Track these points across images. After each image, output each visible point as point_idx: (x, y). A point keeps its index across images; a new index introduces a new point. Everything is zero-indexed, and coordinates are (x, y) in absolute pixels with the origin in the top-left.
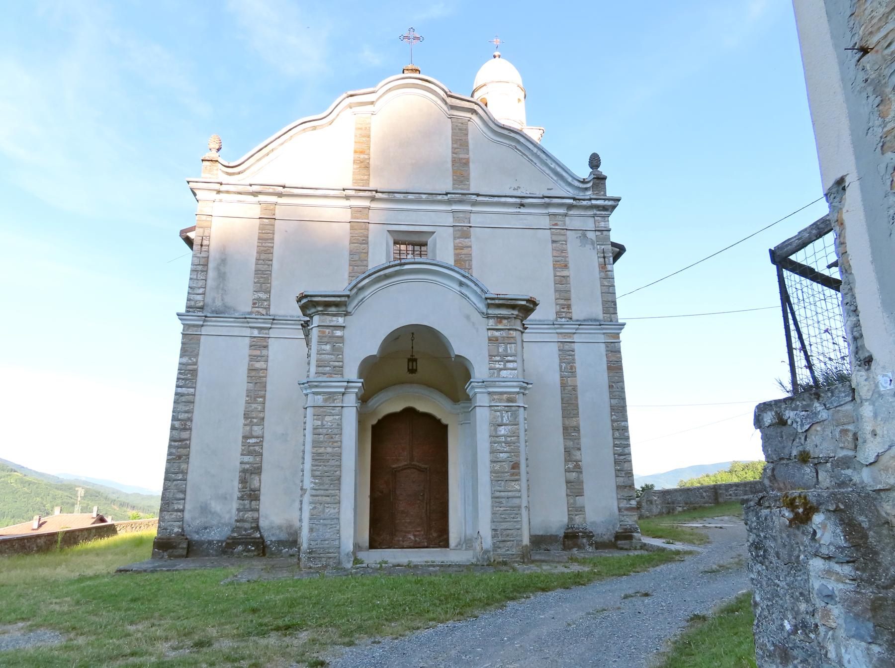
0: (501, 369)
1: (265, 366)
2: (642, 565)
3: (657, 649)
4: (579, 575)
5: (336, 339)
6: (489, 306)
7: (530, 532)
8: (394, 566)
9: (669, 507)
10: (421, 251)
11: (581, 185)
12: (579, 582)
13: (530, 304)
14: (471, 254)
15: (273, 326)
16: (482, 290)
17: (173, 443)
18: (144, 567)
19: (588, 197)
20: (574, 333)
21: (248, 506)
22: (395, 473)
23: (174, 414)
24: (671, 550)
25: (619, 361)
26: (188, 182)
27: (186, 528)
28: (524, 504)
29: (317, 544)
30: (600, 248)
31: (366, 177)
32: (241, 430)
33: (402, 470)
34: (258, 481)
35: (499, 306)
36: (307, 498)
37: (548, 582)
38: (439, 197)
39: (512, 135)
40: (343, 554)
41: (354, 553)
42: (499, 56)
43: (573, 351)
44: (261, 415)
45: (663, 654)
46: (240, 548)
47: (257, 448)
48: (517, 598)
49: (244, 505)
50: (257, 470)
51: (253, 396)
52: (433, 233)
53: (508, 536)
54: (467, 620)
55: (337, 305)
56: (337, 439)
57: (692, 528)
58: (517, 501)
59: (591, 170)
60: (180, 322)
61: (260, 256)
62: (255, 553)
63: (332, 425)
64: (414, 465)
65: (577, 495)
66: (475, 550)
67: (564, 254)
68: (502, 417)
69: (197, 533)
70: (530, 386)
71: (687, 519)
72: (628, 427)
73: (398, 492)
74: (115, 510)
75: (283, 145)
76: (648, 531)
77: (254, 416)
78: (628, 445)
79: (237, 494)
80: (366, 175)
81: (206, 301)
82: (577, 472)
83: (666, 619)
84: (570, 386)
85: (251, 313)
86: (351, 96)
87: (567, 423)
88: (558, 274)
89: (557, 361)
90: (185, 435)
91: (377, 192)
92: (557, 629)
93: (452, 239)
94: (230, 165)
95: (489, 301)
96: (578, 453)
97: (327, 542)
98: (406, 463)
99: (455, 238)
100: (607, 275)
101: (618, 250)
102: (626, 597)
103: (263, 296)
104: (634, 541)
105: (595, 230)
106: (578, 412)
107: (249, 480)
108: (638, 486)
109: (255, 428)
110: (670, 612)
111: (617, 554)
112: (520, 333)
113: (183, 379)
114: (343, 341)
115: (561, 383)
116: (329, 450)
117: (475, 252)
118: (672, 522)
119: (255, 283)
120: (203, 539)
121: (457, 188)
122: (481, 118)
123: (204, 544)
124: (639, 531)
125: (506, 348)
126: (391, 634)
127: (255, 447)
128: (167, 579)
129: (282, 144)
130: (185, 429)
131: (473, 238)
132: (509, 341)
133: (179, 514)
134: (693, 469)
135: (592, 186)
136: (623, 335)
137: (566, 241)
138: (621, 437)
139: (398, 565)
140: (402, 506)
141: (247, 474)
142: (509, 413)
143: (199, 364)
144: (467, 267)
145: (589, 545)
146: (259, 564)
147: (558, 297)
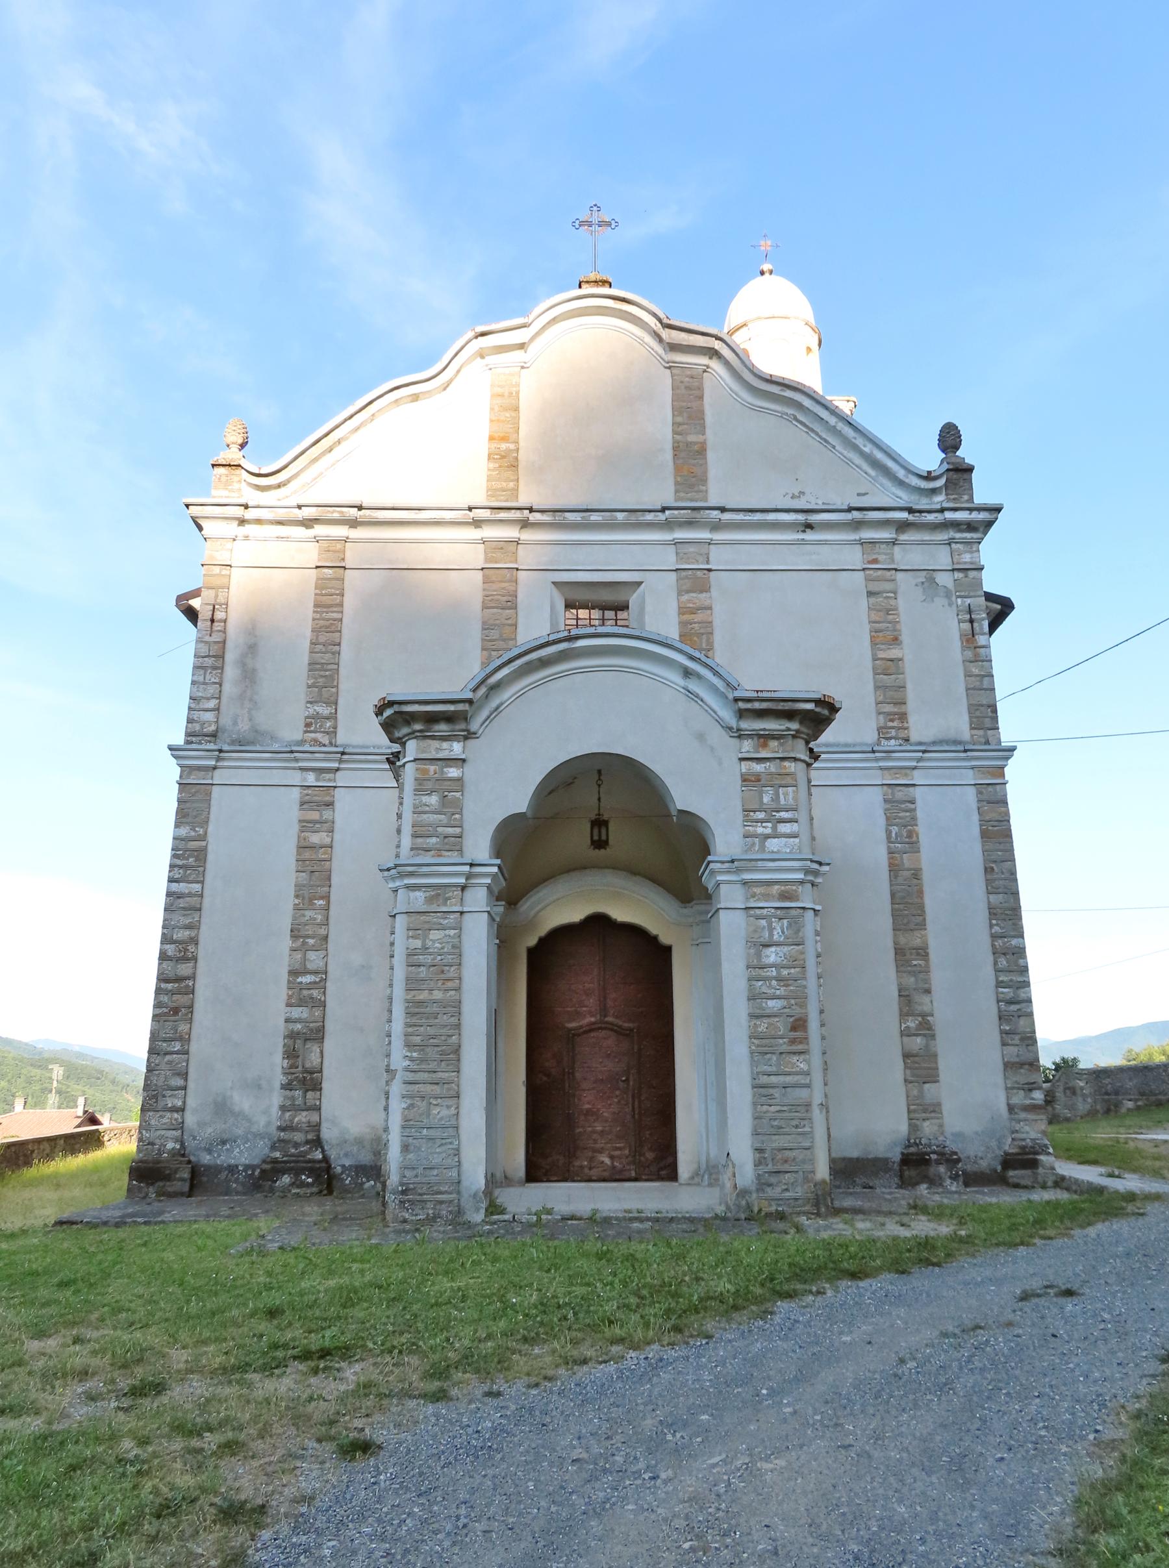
0: (767, 837)
1: (327, 840)
2: (1057, 1224)
3: (1097, 1431)
4: (926, 1243)
5: (449, 783)
6: (741, 714)
7: (830, 1155)
8: (564, 1219)
9: (1109, 1100)
10: (616, 620)
11: (924, 484)
12: (927, 1259)
13: (823, 708)
14: (711, 622)
15: (342, 766)
16: (728, 684)
17: (163, 985)
18: (105, 1215)
19: (938, 507)
20: (915, 768)
21: (299, 1101)
22: (572, 1037)
23: (165, 931)
24: (1117, 1192)
25: (1005, 819)
26: (187, 506)
27: (190, 1144)
28: (818, 1098)
29: (416, 1176)
30: (963, 602)
31: (511, 485)
32: (287, 959)
33: (586, 1032)
34: (318, 1054)
35: (761, 714)
36: (396, 1088)
37: (863, 1258)
38: (650, 517)
39: (788, 394)
40: (465, 1195)
41: (488, 1192)
42: (771, 272)
43: (913, 802)
44: (323, 932)
45: (1112, 1445)
46: (286, 1179)
47: (315, 993)
48: (796, 1295)
49: (293, 1098)
50: (317, 1035)
51: (307, 896)
52: (639, 584)
53: (786, 1161)
54: (687, 1343)
55: (449, 718)
56: (451, 975)
57: (1156, 1144)
58: (803, 1094)
59: (944, 456)
60: (174, 761)
61: (317, 637)
62: (315, 1190)
63: (443, 948)
64: (607, 1023)
65: (925, 1080)
66: (722, 1187)
67: (891, 617)
68: (771, 930)
69: (209, 1151)
70: (825, 868)
71: (1144, 1123)
72: (1024, 948)
73: (578, 1075)
74: (128, 1101)
75: (359, 432)
76: (1068, 1150)
77: (310, 933)
78: (1026, 984)
79: (279, 1078)
80: (512, 481)
81: (222, 721)
82: (924, 1035)
83: (1112, 1352)
84: (908, 870)
85: (302, 742)
86: (483, 334)
87: (902, 940)
88: (881, 655)
89: (882, 821)
90: (184, 969)
91: (531, 510)
92: (874, 1372)
93: (674, 595)
94: (262, 472)
95: (741, 705)
96: (926, 999)
97: (435, 1172)
98: (593, 1019)
99: (680, 593)
100: (976, 655)
101: (999, 607)
102: (1025, 1297)
103: (324, 710)
104: (1040, 1170)
105: (953, 570)
106: (925, 919)
107: (301, 1053)
108: (1047, 1060)
109: (312, 955)
110: (1123, 1335)
111: (1005, 1198)
112: (804, 765)
113: (180, 867)
114: (462, 786)
115: (890, 865)
116: (437, 995)
117: (719, 617)
118: (1115, 1130)
119: (309, 687)
120: (218, 1162)
121: (682, 499)
122: (727, 363)
123: (220, 1172)
124: (1051, 1150)
125: (777, 795)
126: (528, 1374)
127: (312, 991)
128: (138, 1241)
129: (357, 429)
130: (185, 959)
131: (714, 592)
132: (782, 780)
133: (176, 1115)
134: (1151, 1028)
135: (946, 485)
136: (1011, 771)
137: (895, 593)
138: (1011, 968)
139: (573, 1218)
140: (587, 1099)
141: (298, 1041)
142: (785, 921)
143: (210, 838)
144: (704, 646)
145: (950, 1178)
146: (313, 1210)
147: (881, 698)
